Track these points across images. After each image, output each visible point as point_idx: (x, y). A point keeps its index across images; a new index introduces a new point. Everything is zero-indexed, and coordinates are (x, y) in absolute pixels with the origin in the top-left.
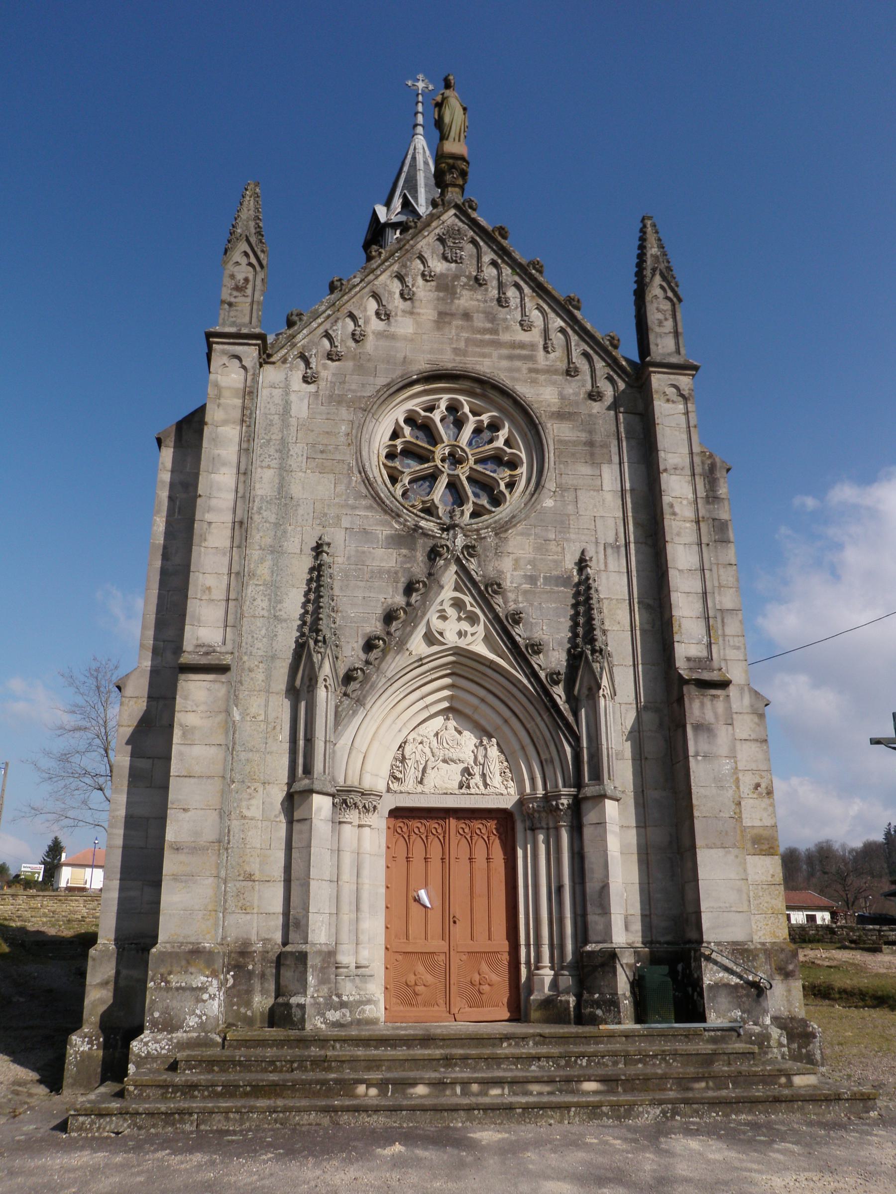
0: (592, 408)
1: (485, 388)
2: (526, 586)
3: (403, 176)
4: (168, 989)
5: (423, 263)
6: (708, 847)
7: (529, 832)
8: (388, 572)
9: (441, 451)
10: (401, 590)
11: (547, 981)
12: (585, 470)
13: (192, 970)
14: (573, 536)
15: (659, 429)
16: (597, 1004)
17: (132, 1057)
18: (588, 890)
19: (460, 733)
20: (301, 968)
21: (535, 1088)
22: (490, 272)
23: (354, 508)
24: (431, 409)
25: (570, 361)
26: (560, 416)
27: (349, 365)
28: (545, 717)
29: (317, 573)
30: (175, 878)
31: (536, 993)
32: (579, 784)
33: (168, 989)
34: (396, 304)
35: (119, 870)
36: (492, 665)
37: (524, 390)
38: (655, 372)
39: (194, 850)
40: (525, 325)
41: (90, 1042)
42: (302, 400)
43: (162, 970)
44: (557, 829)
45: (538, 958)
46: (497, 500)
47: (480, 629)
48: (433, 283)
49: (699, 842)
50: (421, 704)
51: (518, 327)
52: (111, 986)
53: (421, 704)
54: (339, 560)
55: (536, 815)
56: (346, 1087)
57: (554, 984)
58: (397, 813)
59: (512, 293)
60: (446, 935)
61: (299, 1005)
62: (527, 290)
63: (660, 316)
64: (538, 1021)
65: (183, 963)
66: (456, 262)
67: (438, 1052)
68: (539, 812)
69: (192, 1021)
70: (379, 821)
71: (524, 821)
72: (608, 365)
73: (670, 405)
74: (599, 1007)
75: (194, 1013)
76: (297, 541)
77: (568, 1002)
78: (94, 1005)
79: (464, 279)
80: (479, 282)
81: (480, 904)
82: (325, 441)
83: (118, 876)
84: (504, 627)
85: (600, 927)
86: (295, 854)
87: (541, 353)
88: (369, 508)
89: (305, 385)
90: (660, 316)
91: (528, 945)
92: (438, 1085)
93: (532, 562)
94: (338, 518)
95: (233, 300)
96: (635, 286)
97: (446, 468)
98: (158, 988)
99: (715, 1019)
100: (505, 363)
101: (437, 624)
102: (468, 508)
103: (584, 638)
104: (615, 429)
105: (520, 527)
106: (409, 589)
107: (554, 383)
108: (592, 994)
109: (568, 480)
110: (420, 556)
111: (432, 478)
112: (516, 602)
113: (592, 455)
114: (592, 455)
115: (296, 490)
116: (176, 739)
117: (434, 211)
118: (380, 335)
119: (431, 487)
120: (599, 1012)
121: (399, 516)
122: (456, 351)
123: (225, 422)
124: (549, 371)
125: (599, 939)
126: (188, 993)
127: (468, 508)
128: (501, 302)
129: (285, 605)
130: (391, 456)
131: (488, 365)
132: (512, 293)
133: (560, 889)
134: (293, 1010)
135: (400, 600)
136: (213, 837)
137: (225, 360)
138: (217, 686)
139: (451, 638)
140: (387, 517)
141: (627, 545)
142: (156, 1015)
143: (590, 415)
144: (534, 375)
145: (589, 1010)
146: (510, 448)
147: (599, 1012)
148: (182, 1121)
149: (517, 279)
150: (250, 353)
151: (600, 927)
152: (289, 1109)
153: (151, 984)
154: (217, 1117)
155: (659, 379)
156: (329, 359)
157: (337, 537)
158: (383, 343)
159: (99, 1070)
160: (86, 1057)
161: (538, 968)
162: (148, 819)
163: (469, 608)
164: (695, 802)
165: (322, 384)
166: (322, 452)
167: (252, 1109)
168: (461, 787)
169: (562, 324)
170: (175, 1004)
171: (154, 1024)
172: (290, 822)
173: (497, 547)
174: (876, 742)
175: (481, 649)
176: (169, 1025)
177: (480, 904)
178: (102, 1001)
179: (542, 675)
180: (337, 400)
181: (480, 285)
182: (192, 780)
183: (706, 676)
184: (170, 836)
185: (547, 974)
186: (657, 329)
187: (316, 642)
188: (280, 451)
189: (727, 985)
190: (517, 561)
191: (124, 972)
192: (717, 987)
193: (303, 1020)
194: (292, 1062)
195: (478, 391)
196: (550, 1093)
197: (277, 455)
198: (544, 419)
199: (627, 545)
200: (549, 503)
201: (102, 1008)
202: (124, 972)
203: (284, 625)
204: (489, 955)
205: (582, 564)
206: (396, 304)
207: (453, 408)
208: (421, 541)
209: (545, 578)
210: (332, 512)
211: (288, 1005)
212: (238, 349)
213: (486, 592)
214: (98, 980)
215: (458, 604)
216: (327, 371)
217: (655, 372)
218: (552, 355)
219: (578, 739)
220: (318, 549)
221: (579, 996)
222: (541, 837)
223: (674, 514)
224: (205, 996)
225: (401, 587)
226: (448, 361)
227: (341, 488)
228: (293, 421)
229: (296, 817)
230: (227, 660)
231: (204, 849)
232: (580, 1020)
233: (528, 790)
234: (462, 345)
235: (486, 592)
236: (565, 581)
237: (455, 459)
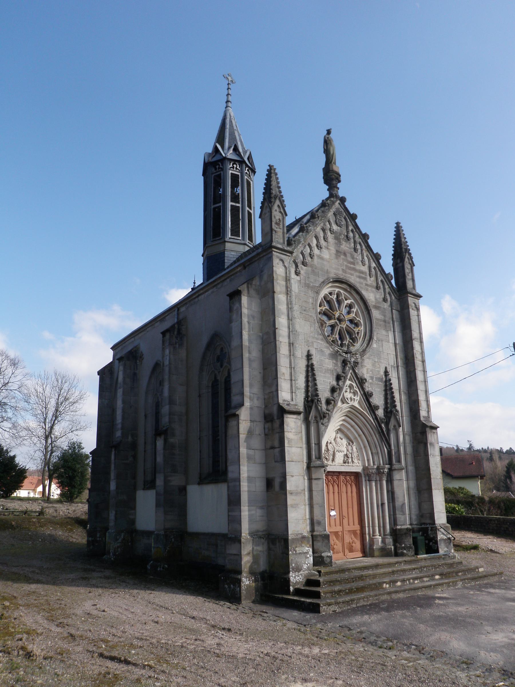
0: (384, 305)
1: (352, 289)
4: (296, 554)
5: (329, 224)
7: (368, 482)
8: (330, 370)
10: (335, 379)
11: (380, 540)
12: (384, 332)
13: (303, 545)
14: (382, 361)
15: (411, 320)
16: (404, 548)
17: (291, 584)
18: (396, 505)
19: (342, 439)
20: (326, 541)
21: (425, 579)
22: (351, 235)
23: (317, 339)
25: (377, 283)
26: (377, 307)
28: (377, 436)
30: (292, 506)
31: (375, 545)
32: (390, 463)
33: (296, 554)
34: (322, 242)
35: (247, 501)
36: (361, 414)
37: (364, 293)
38: (275, 251)
39: (297, 494)
41: (249, 580)
42: (295, 283)
43: (293, 546)
44: (381, 480)
45: (374, 532)
47: (357, 398)
48: (333, 235)
49: (433, 487)
51: (361, 263)
52: (251, 555)
54: (315, 361)
55: (372, 475)
56: (381, 584)
57: (383, 541)
59: (358, 247)
60: (341, 524)
61: (327, 556)
62: (364, 247)
64: (378, 556)
65: (300, 542)
66: (340, 227)
67: (390, 570)
68: (373, 474)
69: (305, 567)
71: (365, 477)
72: (390, 287)
74: (405, 549)
75: (305, 563)
76: (300, 352)
77: (391, 548)
78: (245, 563)
79: (343, 236)
80: (348, 238)
81: (350, 510)
83: (247, 505)
85: (402, 519)
86: (314, 493)
87: (368, 277)
88: (322, 340)
89: (296, 276)
91: (369, 527)
92: (403, 581)
93: (372, 371)
94: (312, 343)
98: (293, 554)
99: (441, 552)
100: (358, 279)
103: (391, 405)
104: (391, 316)
107: (373, 292)
108: (401, 544)
110: (339, 364)
113: (386, 326)
114: (386, 326)
115: (298, 327)
116: (286, 445)
120: (405, 551)
123: (280, 293)
125: (402, 524)
126: (303, 555)
129: (298, 381)
131: (353, 279)
132: (358, 247)
133: (383, 504)
134: (325, 559)
135: (334, 383)
138: (298, 421)
140: (328, 345)
141: (398, 367)
142: (293, 565)
143: (384, 308)
144: (367, 287)
145: (400, 551)
147: (405, 551)
148: (352, 604)
149: (360, 240)
151: (402, 519)
152: (380, 595)
153: (290, 553)
154: (362, 601)
156: (303, 265)
157: (313, 352)
158: (319, 261)
159: (254, 591)
160: (248, 586)
161: (373, 536)
162: (255, 478)
163: (355, 389)
164: (431, 472)
166: (305, 310)
167: (370, 596)
168: (344, 463)
169: (375, 265)
170: (299, 560)
171: (293, 569)
172: (310, 479)
176: (298, 569)
177: (350, 510)
178: (248, 562)
180: (307, 286)
181: (349, 240)
182: (293, 463)
184: (288, 488)
185: (380, 539)
189: (443, 539)
190: (367, 369)
191: (255, 548)
192: (442, 540)
193: (331, 562)
194: (353, 578)
195: (349, 290)
196: (429, 581)
198: (371, 308)
199: (398, 367)
200: (375, 345)
201: (248, 565)
202: (255, 548)
203: (299, 391)
204: (354, 532)
205: (386, 373)
208: (339, 357)
209: (376, 378)
211: (322, 557)
212: (283, 257)
214: (246, 553)
215: (351, 387)
216: (303, 270)
217: (275, 251)
219: (390, 446)
220: (309, 356)
221: (395, 545)
222: (374, 484)
224: (308, 556)
226: (342, 275)
227: (312, 329)
229: (314, 476)
231: (300, 493)
232: (396, 555)
233: (367, 465)
236: (380, 380)
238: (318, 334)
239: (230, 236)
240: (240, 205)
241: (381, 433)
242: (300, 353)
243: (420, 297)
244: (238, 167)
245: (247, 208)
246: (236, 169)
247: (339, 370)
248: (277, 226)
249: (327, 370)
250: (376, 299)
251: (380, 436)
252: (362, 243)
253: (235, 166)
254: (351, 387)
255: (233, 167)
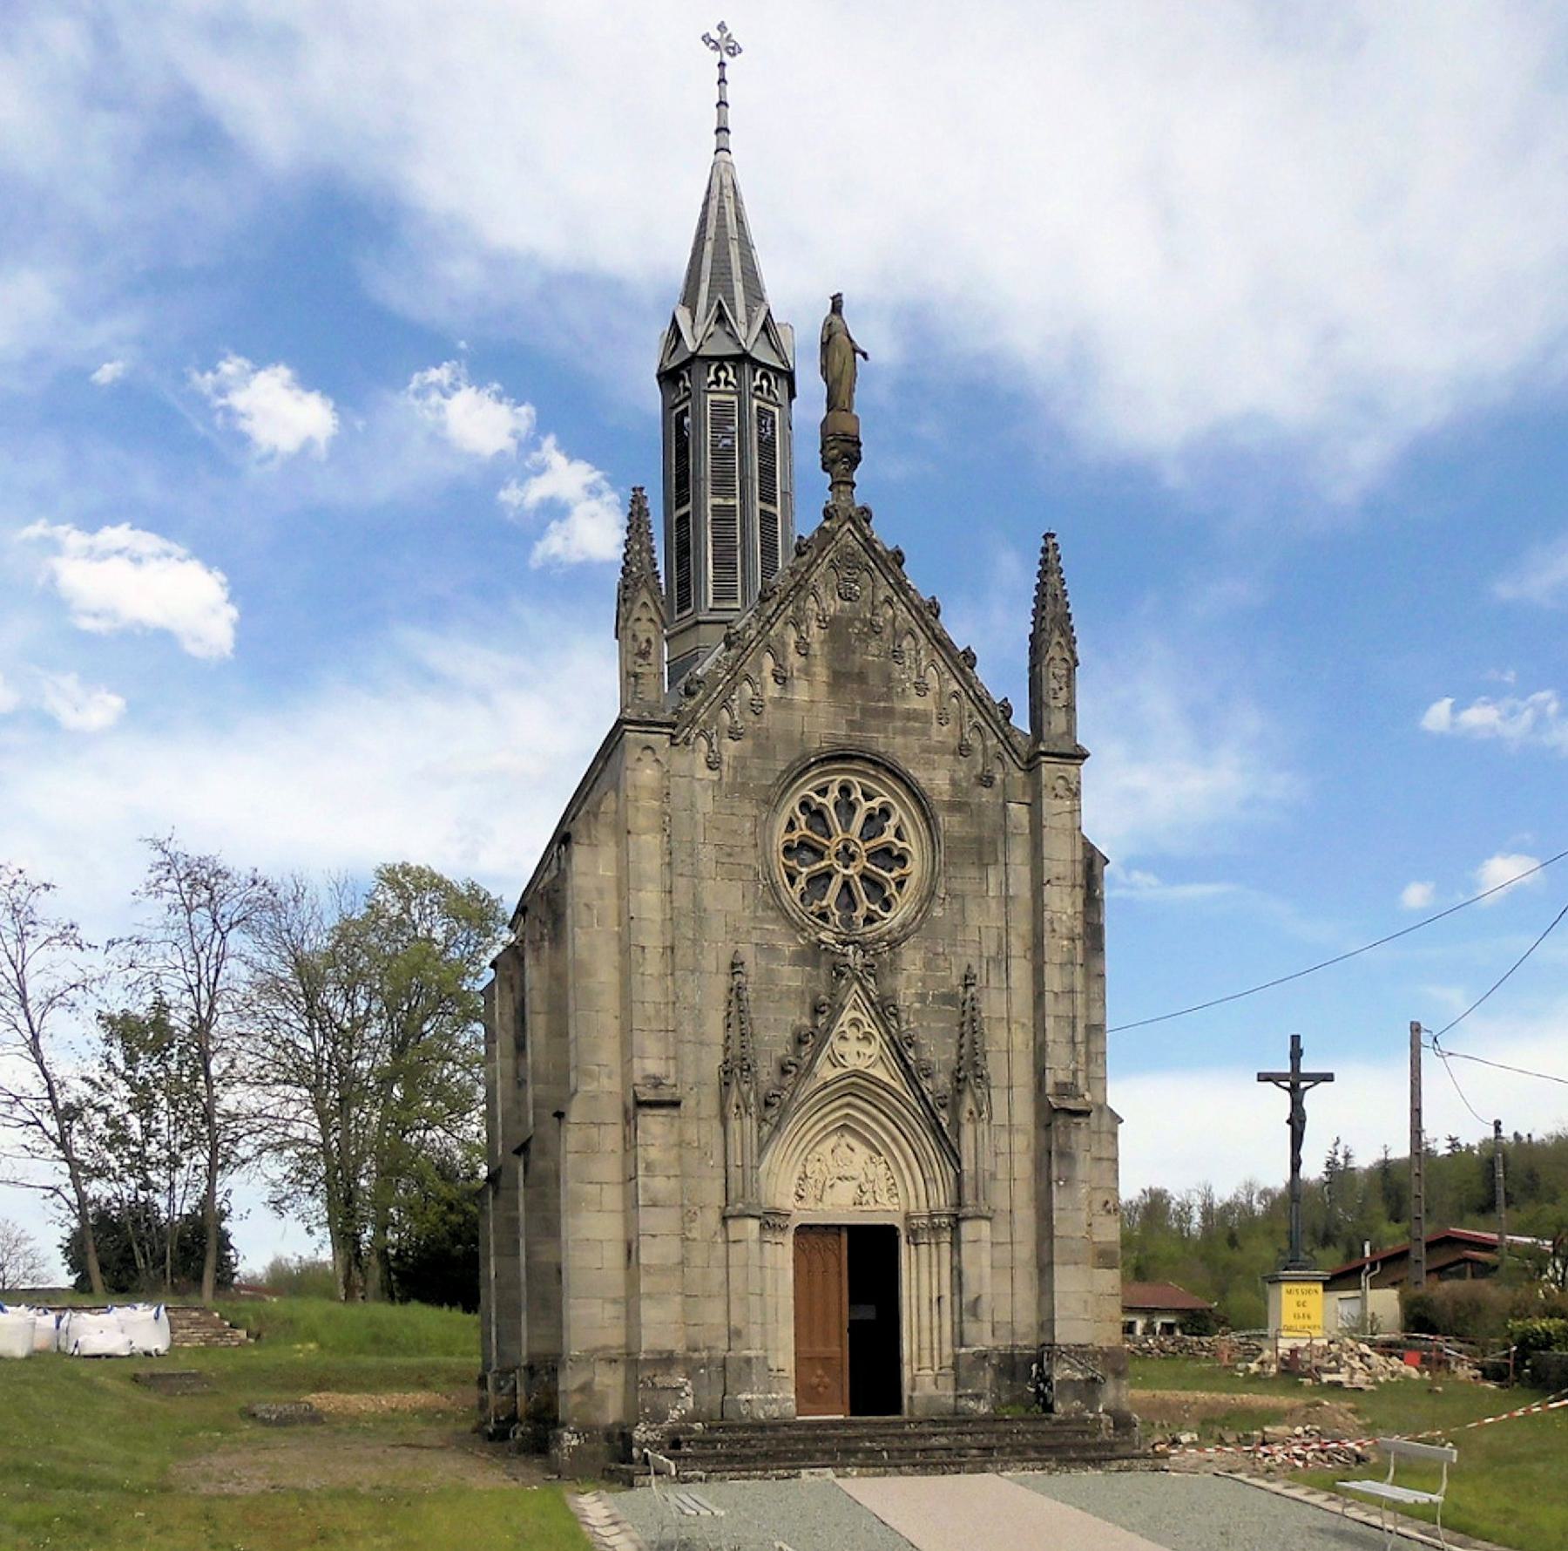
2: (917, 1005)
3: (709, 247)
6: (1064, 1264)
9: (835, 844)
12: (973, 872)
23: (762, 920)
24: (823, 792)
26: (954, 807)
27: (747, 743)
29: (736, 992)
30: (649, 1296)
34: (794, 660)
36: (885, 1087)
37: (918, 774)
40: (921, 689)
42: (706, 790)
46: (887, 905)
50: (822, 1124)
53: (822, 1124)
58: (803, 1230)
63: (1054, 684)
70: (789, 1239)
73: (1058, 801)
82: (732, 842)
84: (899, 1047)
88: (775, 921)
89: (708, 771)
90: (1054, 684)
95: (639, 670)
96: (1031, 629)
97: (838, 865)
101: (840, 1047)
102: (860, 913)
105: (912, 940)
106: (816, 1011)
109: (956, 885)
111: (828, 875)
112: (908, 1022)
115: (708, 901)
117: (827, 524)
118: (777, 702)
119: (826, 887)
121: (803, 930)
122: (851, 723)
124: (941, 749)
127: (860, 913)
128: (897, 655)
130: (788, 850)
136: (676, 1259)
137: (638, 753)
139: (853, 1063)
146: (902, 840)
150: (660, 740)
155: (1049, 771)
157: (748, 953)
165: (724, 768)
166: (730, 855)
173: (893, 962)
174: (1264, 1077)
175: (879, 1073)
179: (930, 1098)
180: (739, 789)
183: (1071, 1104)
186: (1052, 703)
187: (742, 1070)
188: (691, 855)
197: (689, 860)
206: (794, 660)
207: (845, 790)
210: (744, 926)
213: (884, 1010)
218: (945, 728)
223: (1054, 930)
225: (807, 1009)
228: (699, 817)
230: (678, 1093)
234: (857, 716)
235: (884, 1010)
237: (848, 856)
238: (767, 907)
239: (710, 605)
240: (737, 502)
241: (937, 1130)
242: (714, 959)
243: (1085, 756)
244: (731, 378)
245: (759, 505)
246: (727, 383)
247: (822, 988)
248: (640, 661)
249: (787, 994)
250: (954, 783)
251: (936, 1137)
252: (918, 630)
253: (722, 375)
254: (855, 1023)
255: (717, 382)
